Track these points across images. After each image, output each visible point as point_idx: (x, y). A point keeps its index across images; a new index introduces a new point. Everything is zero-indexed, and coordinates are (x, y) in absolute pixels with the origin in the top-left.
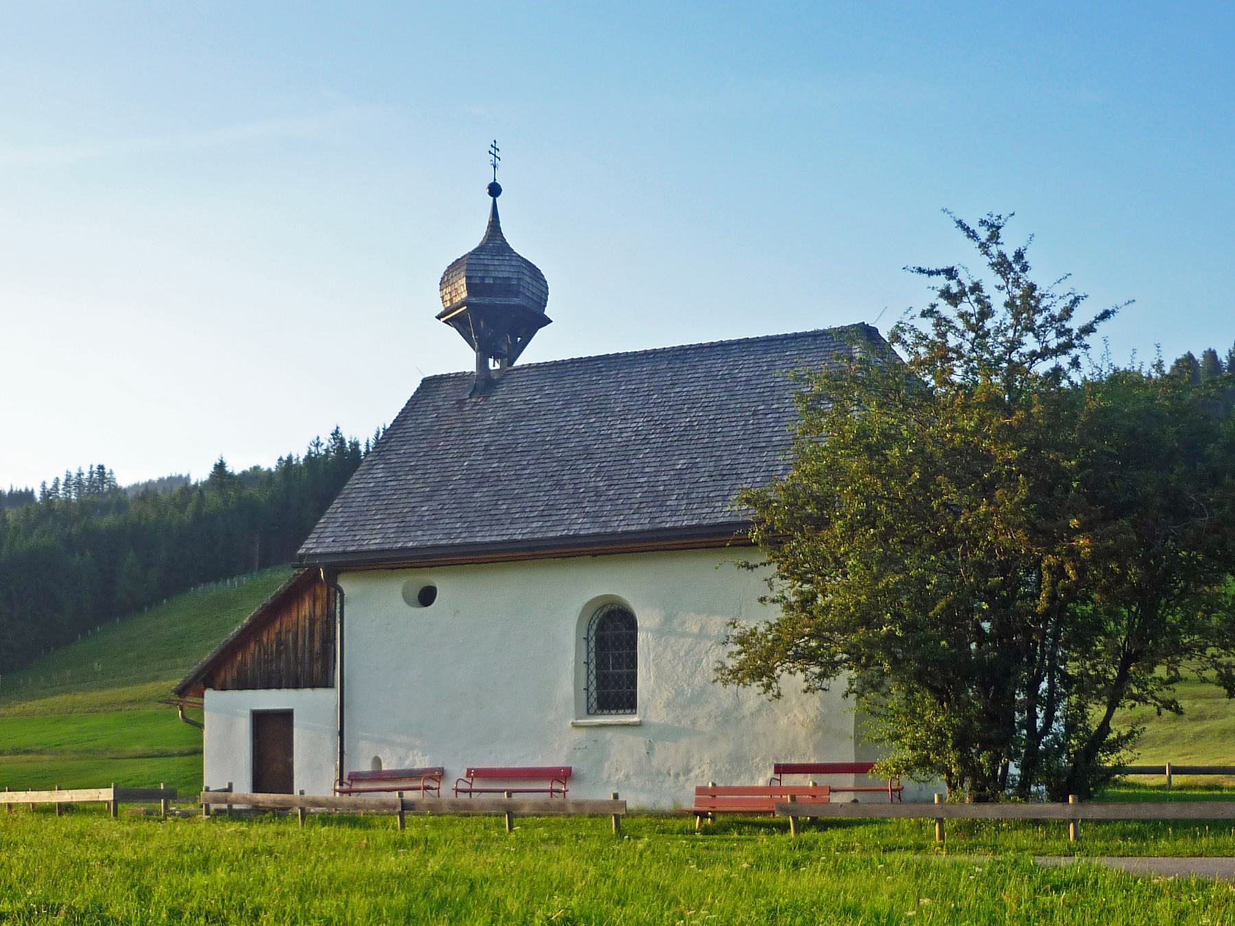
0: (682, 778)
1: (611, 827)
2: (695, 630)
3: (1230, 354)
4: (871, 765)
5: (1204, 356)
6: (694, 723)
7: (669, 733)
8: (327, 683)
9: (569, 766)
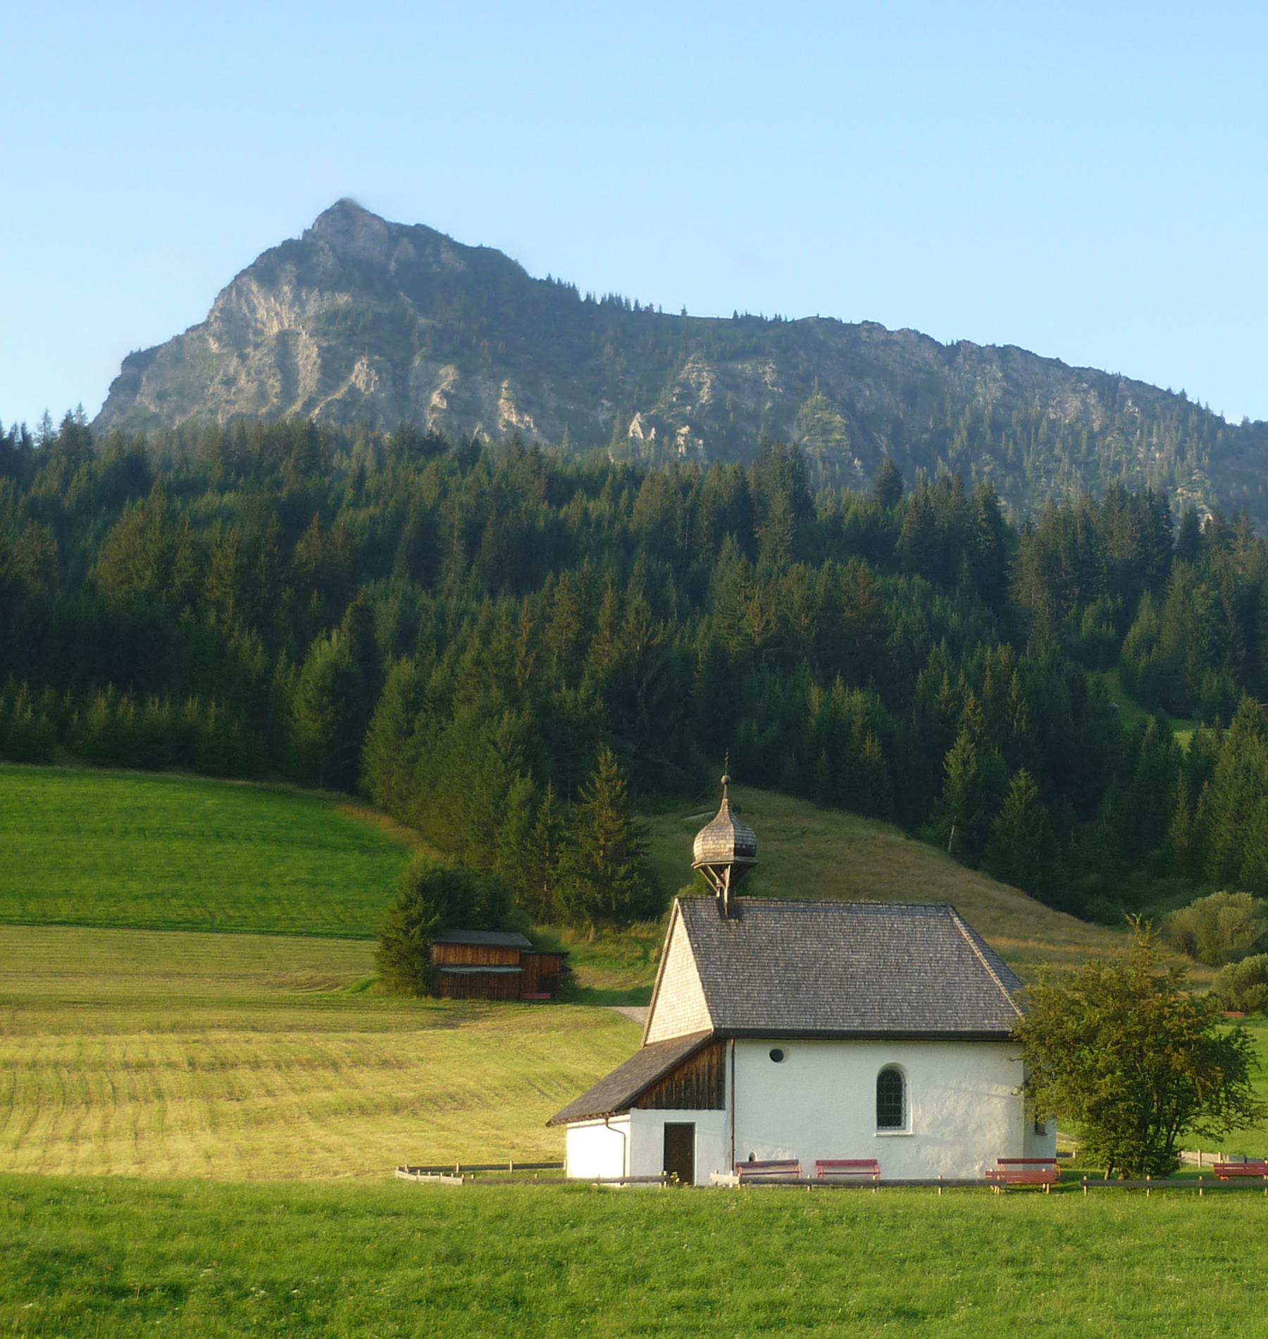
8: (720, 1106)
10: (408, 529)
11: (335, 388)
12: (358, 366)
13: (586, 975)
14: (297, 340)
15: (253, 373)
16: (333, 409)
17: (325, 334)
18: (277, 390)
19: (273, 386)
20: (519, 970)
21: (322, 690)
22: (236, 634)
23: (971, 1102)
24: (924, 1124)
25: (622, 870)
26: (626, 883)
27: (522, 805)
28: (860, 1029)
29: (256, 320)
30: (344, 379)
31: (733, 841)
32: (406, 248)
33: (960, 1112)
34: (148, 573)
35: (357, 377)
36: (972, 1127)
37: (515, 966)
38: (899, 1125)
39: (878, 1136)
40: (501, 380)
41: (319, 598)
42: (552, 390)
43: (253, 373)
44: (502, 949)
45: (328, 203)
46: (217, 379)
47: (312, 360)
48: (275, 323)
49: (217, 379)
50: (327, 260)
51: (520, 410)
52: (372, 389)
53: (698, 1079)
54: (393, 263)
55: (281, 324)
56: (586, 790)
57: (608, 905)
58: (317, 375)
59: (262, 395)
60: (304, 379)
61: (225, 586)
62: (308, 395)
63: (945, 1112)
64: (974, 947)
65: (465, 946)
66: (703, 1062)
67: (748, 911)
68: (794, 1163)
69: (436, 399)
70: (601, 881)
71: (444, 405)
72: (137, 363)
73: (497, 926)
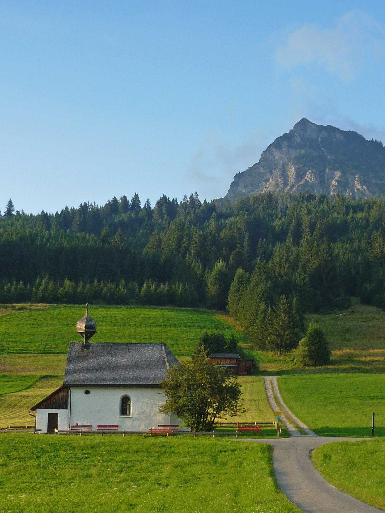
0: (139, 427)
1: (347, 444)
2: (142, 401)
3: (133, 199)
4: (179, 425)
5: (121, 199)
6: (142, 418)
7: (137, 419)
8: (66, 408)
9: (118, 425)
10: (292, 226)
11: (301, 181)
12: (308, 173)
13: (263, 366)
14: (288, 166)
15: (274, 178)
16: (300, 188)
17: (297, 164)
18: (282, 183)
19: (280, 182)
20: (236, 365)
21: (215, 279)
22: (194, 262)
23: (152, 407)
24: (135, 414)
25: (286, 333)
26: (288, 337)
27: (262, 313)
28: (113, 384)
29: (275, 160)
30: (303, 178)
31: (85, 324)
32: (324, 134)
33: (148, 410)
34: (174, 244)
35: (307, 177)
36: (152, 415)
37: (235, 364)
38: (122, 414)
39: (119, 418)
40: (356, 175)
41: (226, 249)
42: (373, 177)
43: (274, 178)
44: (231, 359)
45: (298, 120)
46: (263, 180)
47: (293, 173)
48: (281, 161)
49: (263, 180)
50: (298, 139)
51: (362, 185)
52: (312, 181)
53: (59, 400)
54: (320, 139)
55: (283, 161)
56: (276, 308)
57: (282, 344)
58: (294, 177)
59: (277, 185)
60: (290, 179)
61: (196, 247)
62: (291, 183)
63: (143, 410)
64: (165, 357)
65: (218, 358)
66: (61, 394)
67: (92, 347)
68: (90, 426)
69: (334, 182)
70: (279, 336)
71: (336, 184)
72: (238, 176)
73: (232, 352)
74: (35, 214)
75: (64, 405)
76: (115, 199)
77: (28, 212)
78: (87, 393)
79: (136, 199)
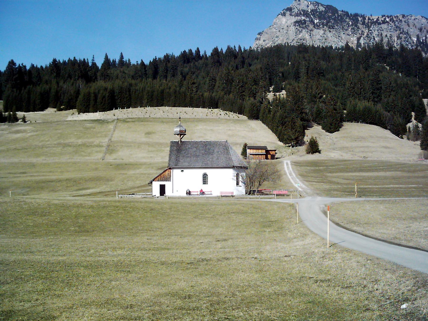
66: (167, 172)
74: (133, 62)
75: (168, 179)
76: (185, 52)
77: (103, 62)
78: (182, 171)
79: (198, 51)
